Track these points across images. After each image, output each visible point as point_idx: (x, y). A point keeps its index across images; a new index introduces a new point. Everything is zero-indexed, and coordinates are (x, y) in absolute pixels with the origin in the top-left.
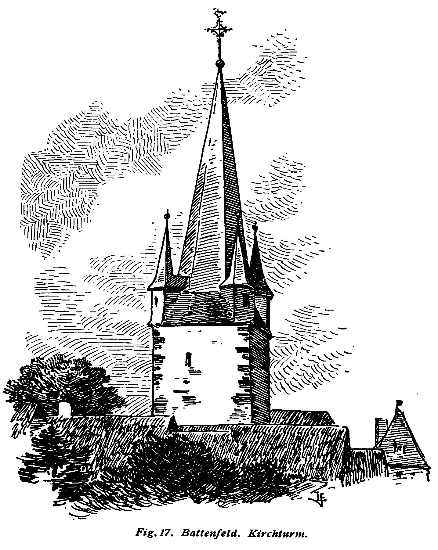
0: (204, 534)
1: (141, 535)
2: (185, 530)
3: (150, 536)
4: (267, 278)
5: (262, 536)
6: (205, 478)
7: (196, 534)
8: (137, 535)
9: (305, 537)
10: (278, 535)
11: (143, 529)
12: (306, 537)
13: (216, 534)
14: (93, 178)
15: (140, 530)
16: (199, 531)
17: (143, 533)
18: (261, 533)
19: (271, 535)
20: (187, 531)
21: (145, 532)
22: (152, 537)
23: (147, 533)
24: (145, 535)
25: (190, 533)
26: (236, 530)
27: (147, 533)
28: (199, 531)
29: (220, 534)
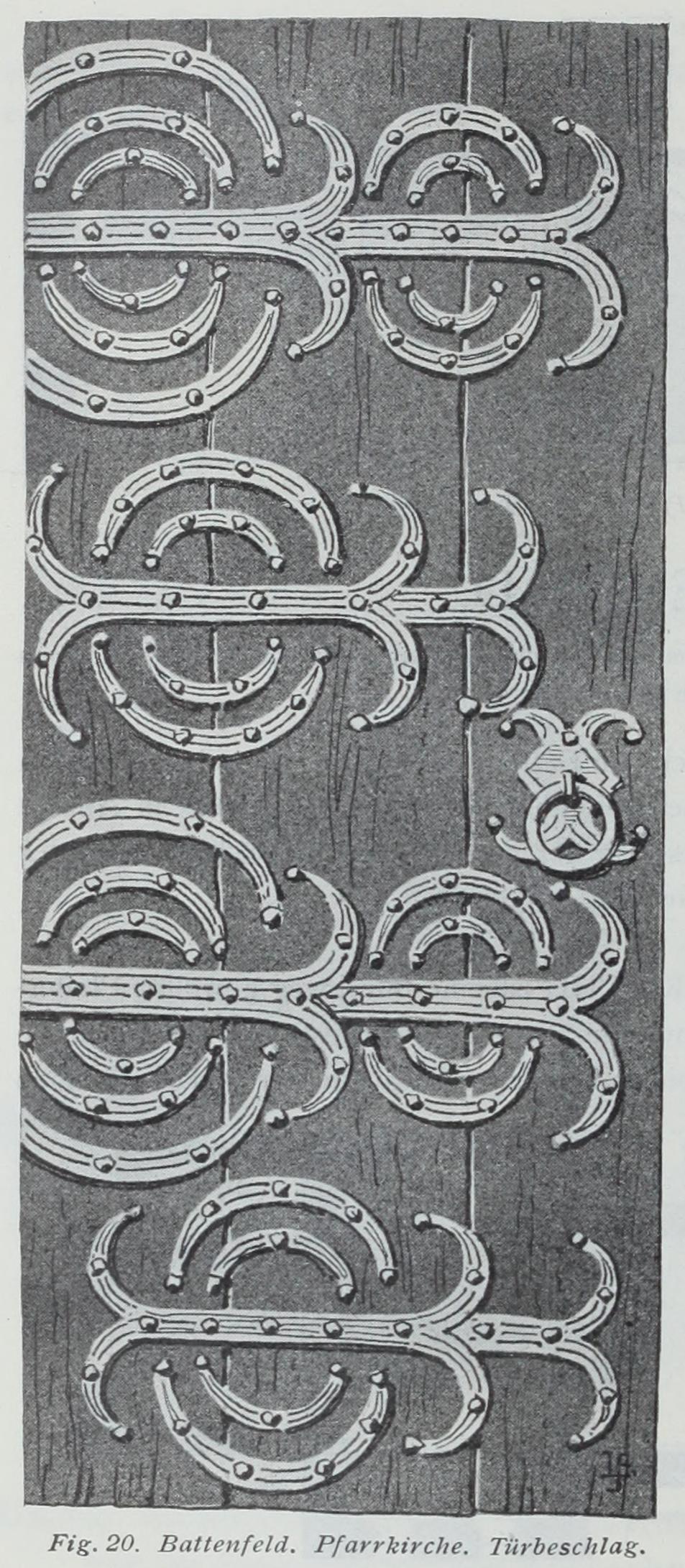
0: (211, 1545)
1: (62, 1549)
2: (167, 1537)
3: (83, 1551)
4: (73, 610)
5: (413, 1551)
6: (576, 1416)
7: (193, 1546)
8: (53, 1549)
9: (288, 1552)
10: (599, 1549)
11: (66, 1535)
12: (293, 1551)
13: (241, 1546)
14: (379, 603)
15: (60, 1539)
16: (199, 1540)
17: (66, 1544)
18: (410, 1543)
19: (433, 1548)
20: (171, 1540)
21: (71, 1542)
22: (87, 1554)
23: (76, 1546)
24: (70, 1549)
25: (178, 1545)
26: (286, 1538)
27: (76, 1546)
28: (199, 1540)
29: (250, 1546)
